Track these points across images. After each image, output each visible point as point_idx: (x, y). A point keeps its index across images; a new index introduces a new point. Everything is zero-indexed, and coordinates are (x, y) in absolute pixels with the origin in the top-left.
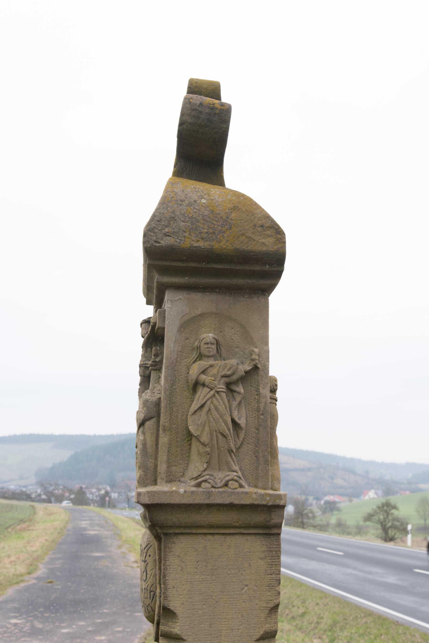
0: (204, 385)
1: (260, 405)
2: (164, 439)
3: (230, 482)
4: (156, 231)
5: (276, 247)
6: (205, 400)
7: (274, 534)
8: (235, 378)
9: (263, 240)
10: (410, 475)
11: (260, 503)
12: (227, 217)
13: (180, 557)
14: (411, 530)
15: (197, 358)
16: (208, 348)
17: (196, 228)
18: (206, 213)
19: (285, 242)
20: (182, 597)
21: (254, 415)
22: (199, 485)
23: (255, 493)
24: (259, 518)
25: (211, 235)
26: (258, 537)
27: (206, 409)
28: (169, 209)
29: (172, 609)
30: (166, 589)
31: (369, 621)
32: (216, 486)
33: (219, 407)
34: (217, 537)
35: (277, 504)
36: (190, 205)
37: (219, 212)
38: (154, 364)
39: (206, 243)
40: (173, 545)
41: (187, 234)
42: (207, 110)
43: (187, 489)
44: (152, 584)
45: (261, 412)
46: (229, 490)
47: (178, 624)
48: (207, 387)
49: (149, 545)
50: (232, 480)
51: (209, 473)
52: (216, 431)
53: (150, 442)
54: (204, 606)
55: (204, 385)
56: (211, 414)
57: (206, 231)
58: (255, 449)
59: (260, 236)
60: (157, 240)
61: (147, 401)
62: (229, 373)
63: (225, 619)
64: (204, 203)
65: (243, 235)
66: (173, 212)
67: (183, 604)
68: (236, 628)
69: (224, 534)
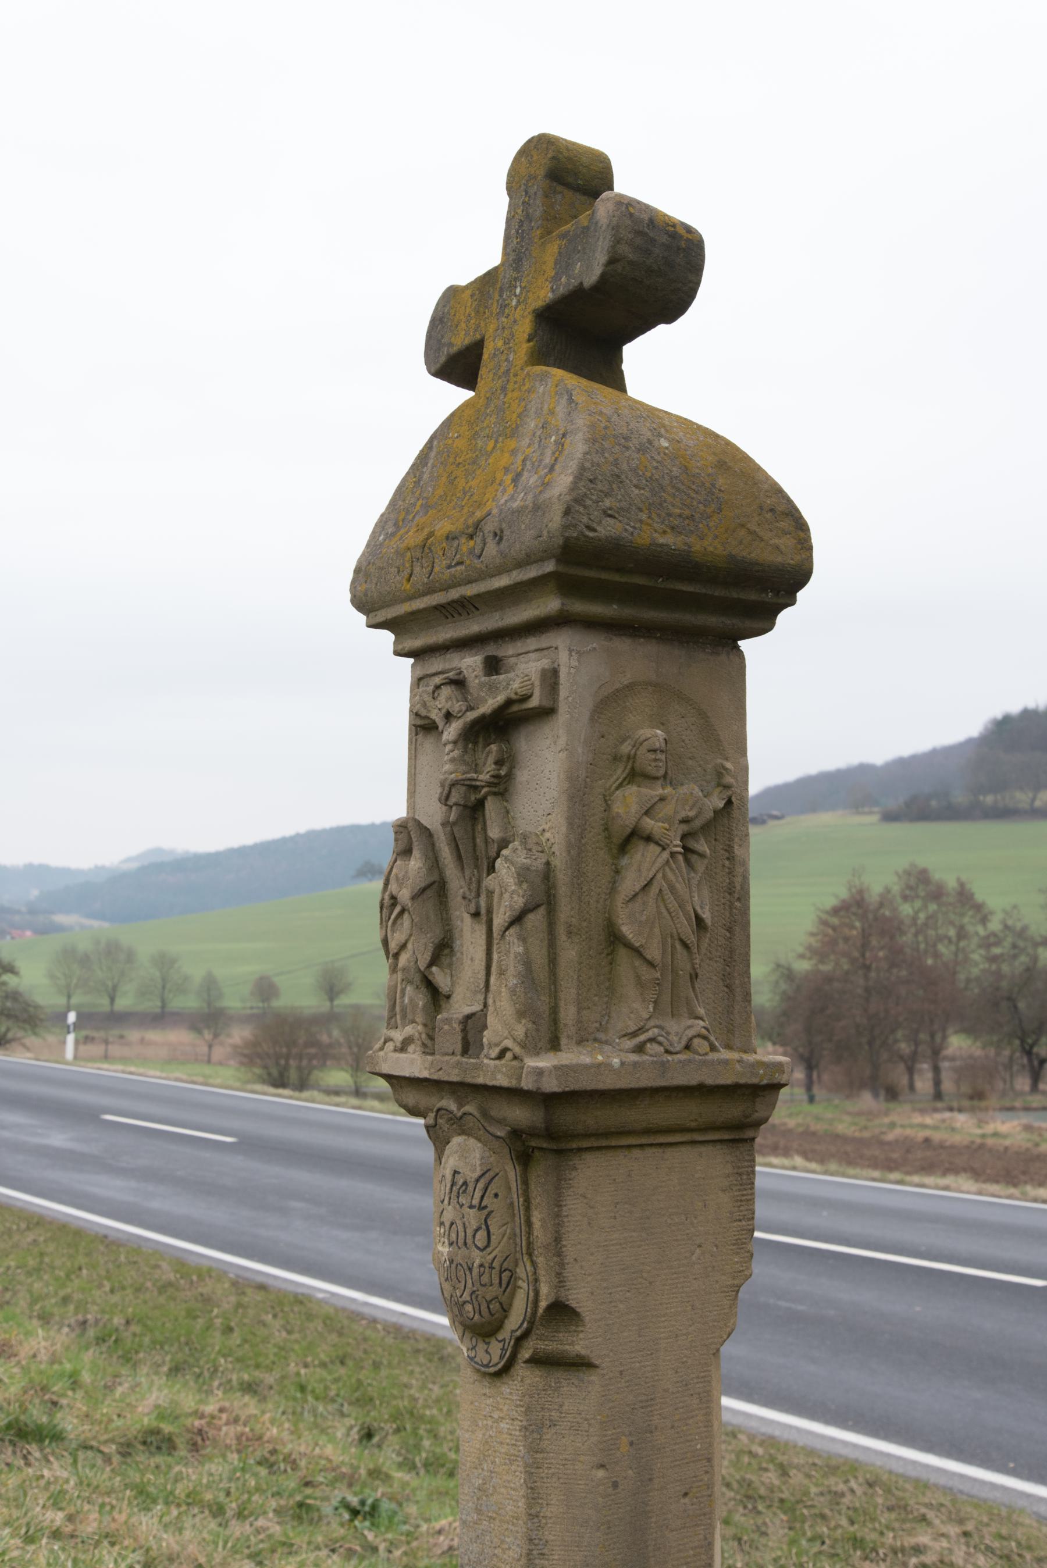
0: (649, 839)
1: (735, 879)
2: (569, 953)
3: (696, 1041)
4: (588, 502)
5: (798, 558)
6: (654, 871)
7: (745, 1140)
8: (698, 823)
9: (776, 541)
10: (35, 893)
11: (750, 1082)
12: (713, 485)
13: (585, 1197)
14: (74, 1024)
15: (624, 779)
16: (656, 760)
17: (661, 504)
18: (676, 471)
19: (811, 548)
20: (589, 1279)
21: (723, 901)
22: (640, 1049)
23: (739, 1061)
24: (732, 1111)
25: (687, 522)
26: (719, 1146)
27: (654, 890)
28: (606, 455)
29: (573, 1306)
30: (563, 1264)
31: (42, 1239)
32: (672, 1049)
33: (677, 885)
34: (650, 1151)
35: (775, 1081)
36: (642, 449)
37: (697, 471)
38: (496, 781)
39: (679, 539)
40: (574, 1173)
41: (644, 516)
42: (664, 239)
43: (624, 1059)
44: (505, 1255)
45: (736, 895)
46: (697, 1057)
47: (581, 1336)
48: (657, 843)
49: (488, 1176)
50: (699, 1036)
51: (658, 1023)
52: (672, 937)
53: (539, 957)
54: (628, 1294)
55: (649, 839)
56: (663, 900)
57: (678, 511)
58: (725, 970)
59: (771, 531)
60: (590, 523)
61: (528, 869)
62: (691, 814)
63: (664, 1316)
64: (667, 448)
65: (743, 526)
66: (616, 463)
67: (592, 1293)
68: (684, 1332)
69: (661, 1145)
